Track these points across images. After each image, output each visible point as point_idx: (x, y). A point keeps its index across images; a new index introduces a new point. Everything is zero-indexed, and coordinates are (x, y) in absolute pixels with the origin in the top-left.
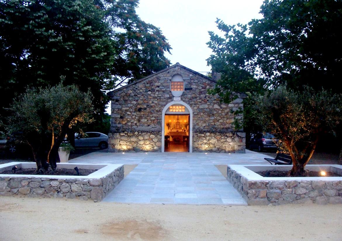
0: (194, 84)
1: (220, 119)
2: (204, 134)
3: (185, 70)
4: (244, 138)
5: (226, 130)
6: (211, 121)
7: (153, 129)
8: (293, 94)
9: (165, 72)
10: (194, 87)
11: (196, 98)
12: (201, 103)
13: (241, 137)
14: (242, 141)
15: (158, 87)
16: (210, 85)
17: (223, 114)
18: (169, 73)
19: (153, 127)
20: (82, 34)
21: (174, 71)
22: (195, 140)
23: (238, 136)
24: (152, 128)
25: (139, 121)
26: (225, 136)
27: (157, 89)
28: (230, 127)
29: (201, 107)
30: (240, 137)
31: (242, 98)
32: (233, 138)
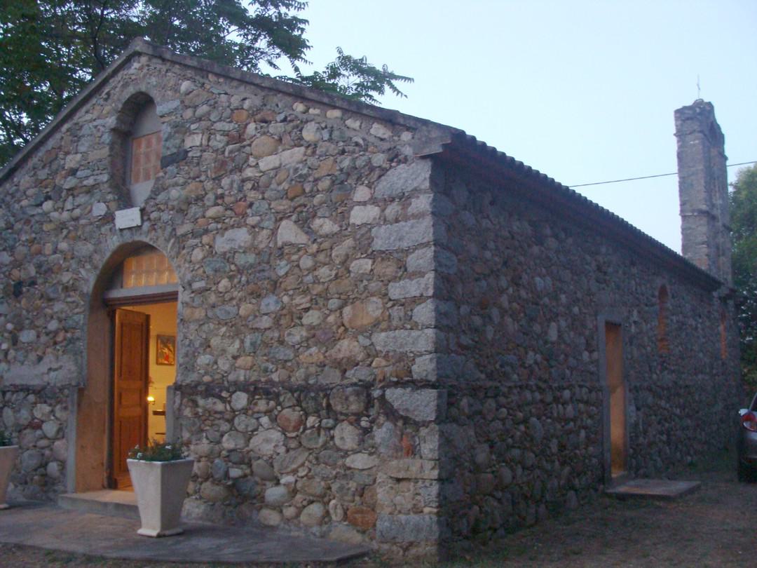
0: (193, 127)
1: (307, 310)
2: (223, 400)
3: (167, 538)
4: (425, 424)
5: (338, 373)
6: (266, 322)
7: (52, 374)
8: (488, 254)
9: (94, 101)
10: (194, 141)
11: (200, 199)
12: (219, 226)
13: (406, 420)
14: (413, 451)
15: (73, 172)
16: (258, 117)
17: (324, 272)
18: (110, 101)
19: (55, 366)
20: (167, 447)
21: (125, 85)
22: (372, 347)
23: (391, 413)
24: (50, 369)
25: (15, 341)
26: (324, 413)
27: (71, 182)
28: (360, 357)
29: (221, 245)
30: (400, 423)
31: (424, 158)
32: (364, 423)
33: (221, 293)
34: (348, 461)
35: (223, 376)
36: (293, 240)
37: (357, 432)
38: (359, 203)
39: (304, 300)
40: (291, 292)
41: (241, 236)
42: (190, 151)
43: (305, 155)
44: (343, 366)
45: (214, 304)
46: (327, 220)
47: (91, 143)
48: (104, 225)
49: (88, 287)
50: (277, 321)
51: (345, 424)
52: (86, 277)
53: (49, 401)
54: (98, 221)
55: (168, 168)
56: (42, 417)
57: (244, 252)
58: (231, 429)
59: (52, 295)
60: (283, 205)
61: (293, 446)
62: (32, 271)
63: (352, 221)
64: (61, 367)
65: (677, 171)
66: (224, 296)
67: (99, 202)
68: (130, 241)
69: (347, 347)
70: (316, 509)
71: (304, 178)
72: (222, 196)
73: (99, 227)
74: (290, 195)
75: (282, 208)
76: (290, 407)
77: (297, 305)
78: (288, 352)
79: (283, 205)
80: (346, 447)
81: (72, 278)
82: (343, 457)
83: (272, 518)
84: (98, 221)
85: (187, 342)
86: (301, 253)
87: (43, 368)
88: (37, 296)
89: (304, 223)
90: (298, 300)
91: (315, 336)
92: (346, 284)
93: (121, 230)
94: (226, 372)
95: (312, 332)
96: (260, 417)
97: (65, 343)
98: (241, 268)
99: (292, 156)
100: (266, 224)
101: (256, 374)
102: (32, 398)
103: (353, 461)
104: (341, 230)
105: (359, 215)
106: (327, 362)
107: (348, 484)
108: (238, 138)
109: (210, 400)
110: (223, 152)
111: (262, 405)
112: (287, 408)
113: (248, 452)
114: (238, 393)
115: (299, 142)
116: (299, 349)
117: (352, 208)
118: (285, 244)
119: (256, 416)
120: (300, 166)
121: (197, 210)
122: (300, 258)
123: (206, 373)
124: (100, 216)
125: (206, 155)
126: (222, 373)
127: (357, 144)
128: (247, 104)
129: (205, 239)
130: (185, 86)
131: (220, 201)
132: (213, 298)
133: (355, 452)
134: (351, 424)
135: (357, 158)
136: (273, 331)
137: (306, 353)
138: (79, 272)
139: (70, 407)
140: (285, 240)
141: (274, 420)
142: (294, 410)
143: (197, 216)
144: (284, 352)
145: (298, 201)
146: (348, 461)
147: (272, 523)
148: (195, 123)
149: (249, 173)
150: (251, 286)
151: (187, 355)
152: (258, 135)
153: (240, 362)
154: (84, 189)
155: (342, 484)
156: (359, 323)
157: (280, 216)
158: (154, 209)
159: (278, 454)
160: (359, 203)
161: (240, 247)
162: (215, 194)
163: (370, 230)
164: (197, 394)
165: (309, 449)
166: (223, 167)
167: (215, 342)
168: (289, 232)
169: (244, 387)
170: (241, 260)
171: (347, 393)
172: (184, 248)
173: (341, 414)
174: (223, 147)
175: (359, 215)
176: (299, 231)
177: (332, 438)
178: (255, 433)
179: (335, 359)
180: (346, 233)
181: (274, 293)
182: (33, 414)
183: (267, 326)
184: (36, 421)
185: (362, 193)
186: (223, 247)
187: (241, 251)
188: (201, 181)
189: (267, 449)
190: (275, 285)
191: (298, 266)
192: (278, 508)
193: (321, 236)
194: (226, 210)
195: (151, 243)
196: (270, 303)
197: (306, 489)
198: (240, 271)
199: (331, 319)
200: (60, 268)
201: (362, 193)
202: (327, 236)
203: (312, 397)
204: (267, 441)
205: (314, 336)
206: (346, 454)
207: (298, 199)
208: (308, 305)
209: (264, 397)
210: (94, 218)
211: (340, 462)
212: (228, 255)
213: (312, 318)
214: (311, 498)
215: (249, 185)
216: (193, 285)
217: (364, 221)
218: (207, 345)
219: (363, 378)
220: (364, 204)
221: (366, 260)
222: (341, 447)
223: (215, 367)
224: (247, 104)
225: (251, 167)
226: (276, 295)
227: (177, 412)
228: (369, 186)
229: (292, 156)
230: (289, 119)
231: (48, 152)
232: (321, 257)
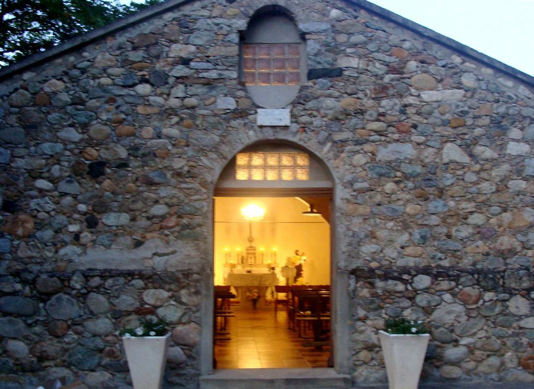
1: (471, 213)
2: (405, 282)
12: (383, 138)
17: (486, 186)
24: (155, 254)
27: (180, 71)
29: (385, 154)
33: (387, 194)
34: (522, 323)
35: (391, 262)
36: (458, 159)
37: (528, 302)
38: (514, 140)
39: (469, 206)
40: (457, 199)
41: (408, 150)
42: (345, 70)
43: (465, 96)
44: (504, 254)
45: (380, 202)
46: (487, 148)
47: (210, 38)
48: (235, 118)
49: (213, 176)
50: (444, 220)
51: (518, 297)
52: (211, 166)
53: (167, 287)
54: (224, 114)
55: (320, 80)
56: (156, 302)
57: (410, 163)
58: (412, 306)
59: (157, 180)
60: (448, 131)
61: (473, 315)
62: (123, 153)
63: (508, 151)
64: (174, 253)
65: (277, 156)
66: (390, 196)
67: (226, 95)
68: (272, 138)
69: (506, 241)
70: (494, 361)
71: (464, 113)
72: (383, 115)
73: (228, 120)
74: (454, 125)
75: (447, 133)
76: (470, 286)
77: (463, 209)
78: (456, 244)
79: (448, 131)
80: (520, 314)
81: (186, 165)
82: (517, 320)
83: (454, 372)
84: (224, 114)
85: (351, 233)
86: (465, 170)
87: (143, 252)
88: (129, 179)
89: (467, 147)
90: (464, 205)
91: (481, 233)
92: (505, 197)
93: (261, 127)
94: (394, 259)
95: (478, 229)
96: (442, 294)
97: (177, 229)
98: (408, 176)
99: (452, 96)
100: (432, 144)
101: (425, 260)
102: (139, 283)
103: (526, 323)
104: (499, 157)
105: (513, 149)
106: (491, 252)
107: (521, 339)
108: (397, 70)
109: (390, 282)
110: (382, 78)
111: (445, 284)
112: (468, 286)
113: (429, 322)
114: (421, 276)
115: (459, 86)
116: (466, 242)
117: (508, 142)
118: (451, 162)
119: (438, 293)
120: (461, 104)
121: (358, 122)
122: (465, 173)
123: (374, 259)
124: (229, 109)
125: (363, 77)
126: (390, 259)
127: (510, 97)
128: (407, 45)
129: (368, 147)
130: (334, 13)
131: (382, 118)
132: (378, 198)
133: (527, 316)
134: (523, 296)
135: (510, 107)
136: (441, 227)
137: (473, 246)
138: (200, 160)
139: (204, 292)
140: (451, 159)
141: (454, 295)
142: (473, 288)
143: (357, 127)
144: (452, 245)
145: (461, 130)
146: (522, 323)
147: (454, 376)
148: (351, 48)
149: (410, 100)
150: (418, 191)
151: (350, 244)
152: (419, 72)
153: (408, 251)
154: (202, 81)
155: (516, 341)
156: (516, 225)
157: (445, 139)
158: (302, 113)
159: (459, 322)
160: (514, 140)
161: (406, 158)
162: (377, 111)
163: (523, 161)
164: (375, 278)
165: (485, 317)
166: (382, 92)
167: (382, 234)
168: (453, 152)
169: (426, 271)
170: (407, 169)
171: (521, 275)
172: (342, 152)
173: (515, 290)
174: (383, 74)
175: (513, 149)
176: (463, 153)
177: (507, 307)
178: (438, 307)
179: (499, 250)
180: (504, 159)
181: (440, 197)
182: (142, 299)
183: (436, 223)
184: (147, 306)
185: (515, 133)
186: (388, 157)
187: (407, 162)
188: (358, 98)
189: (449, 319)
190: (441, 193)
191: (463, 180)
192: (456, 363)
193: (483, 160)
194: (389, 126)
195: (301, 143)
196: (437, 205)
197: (485, 346)
198: (407, 177)
199: (493, 221)
200: (168, 153)
201: (515, 133)
202: (487, 160)
203: (491, 278)
204: (449, 313)
205: (479, 233)
206: (520, 318)
207: (460, 128)
208: (474, 209)
209: (446, 278)
210: (220, 110)
211: (515, 325)
212: (393, 164)
213: (477, 219)
214: (489, 353)
215: (413, 110)
216: (354, 184)
217: (519, 153)
218: (372, 236)
219: (522, 264)
220: (518, 141)
221: (521, 181)
222: (516, 314)
223: (382, 255)
224: (407, 45)
225: (413, 96)
226: (444, 200)
227: (352, 294)
228: (522, 129)
229: (452, 96)
230: (450, 66)
231: (142, 35)
232: (484, 175)
